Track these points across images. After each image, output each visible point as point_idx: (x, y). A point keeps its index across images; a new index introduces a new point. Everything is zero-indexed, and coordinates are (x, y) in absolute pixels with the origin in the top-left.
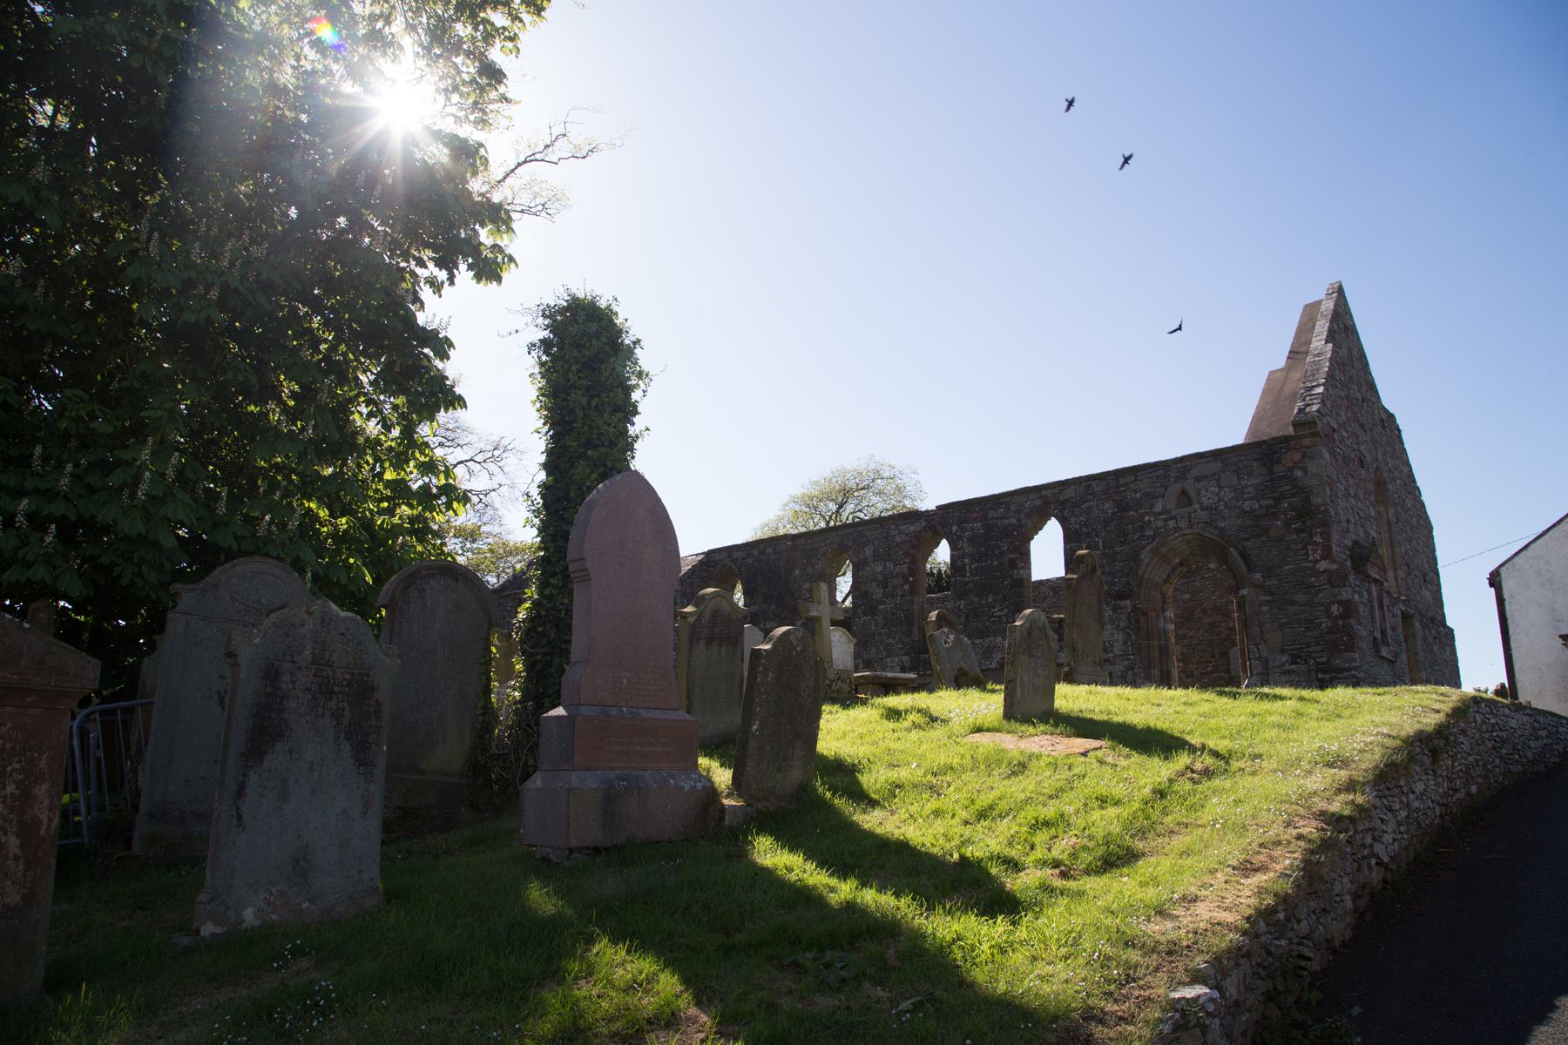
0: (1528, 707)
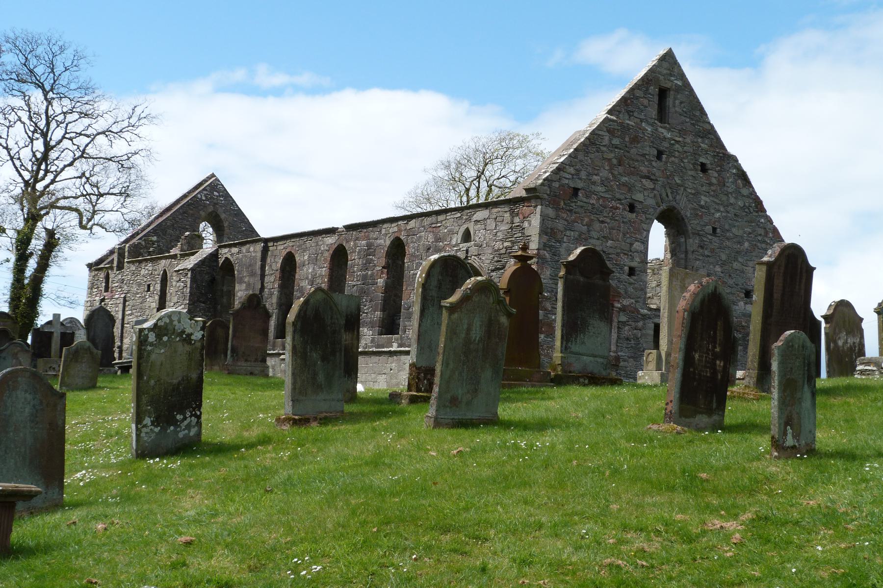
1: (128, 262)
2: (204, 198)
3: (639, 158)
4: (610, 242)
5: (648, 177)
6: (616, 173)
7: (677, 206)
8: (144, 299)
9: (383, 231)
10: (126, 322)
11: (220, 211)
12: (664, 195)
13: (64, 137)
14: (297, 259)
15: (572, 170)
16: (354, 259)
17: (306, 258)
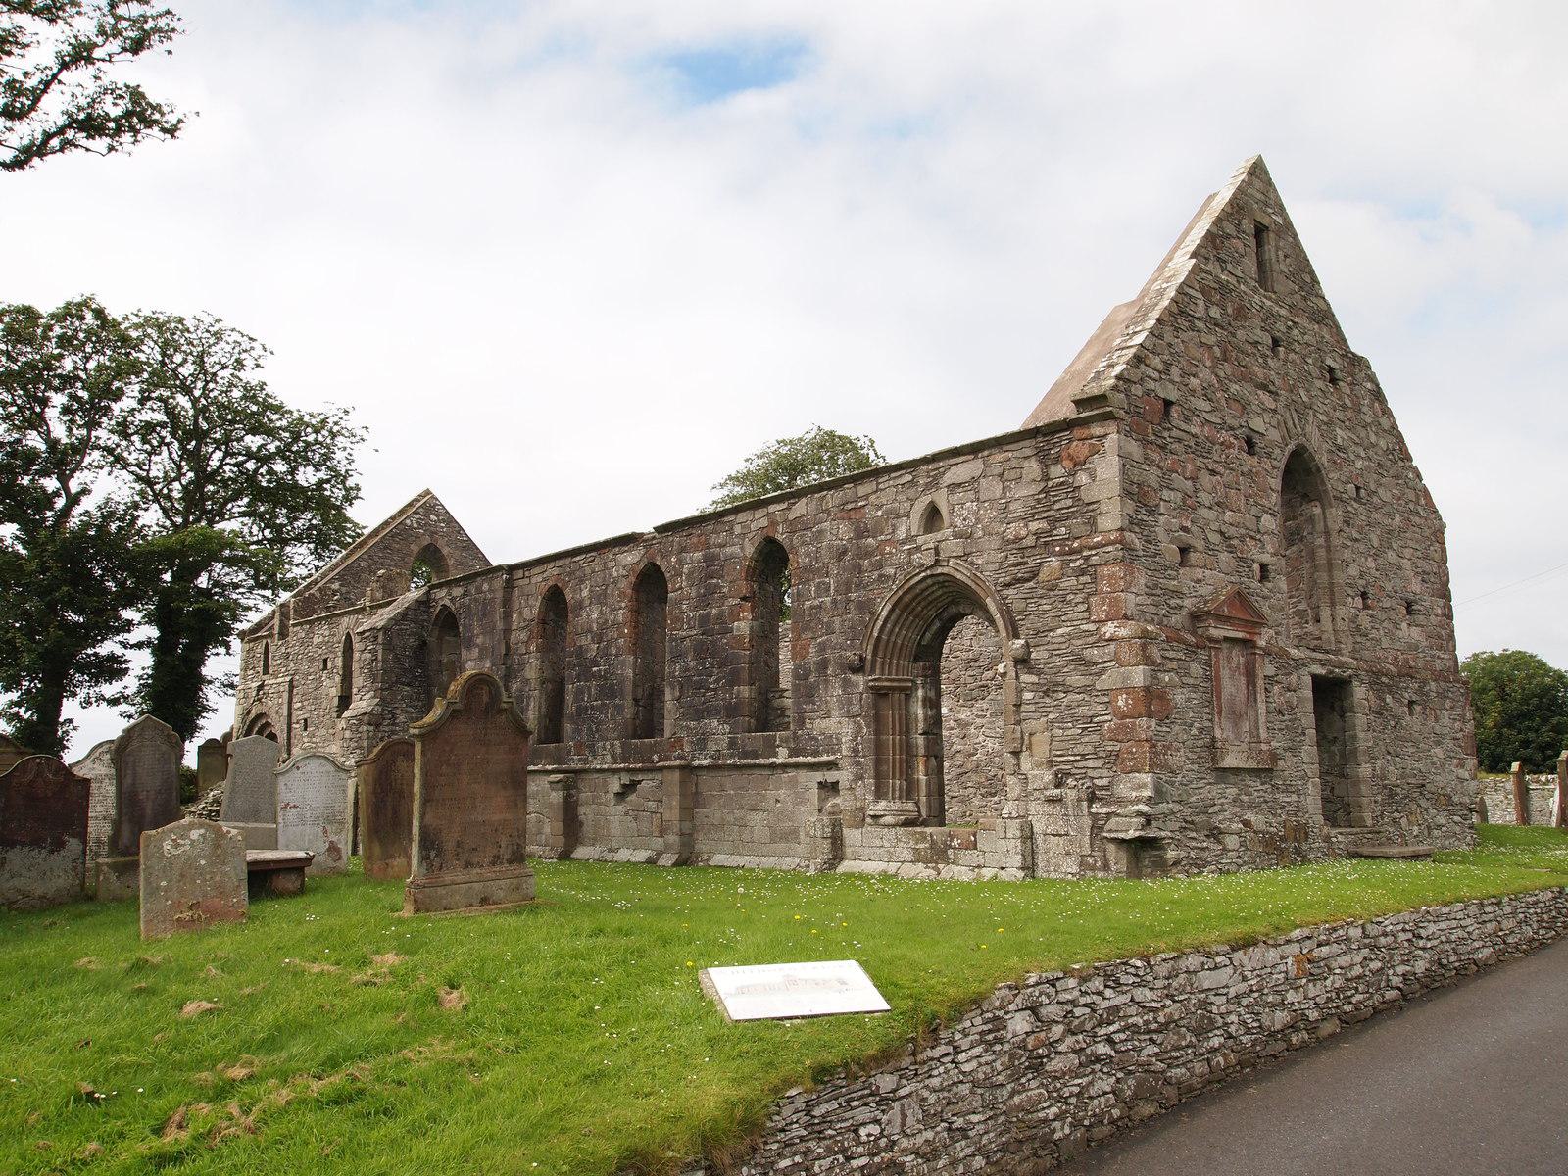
0: (500, 568)
1: (294, 626)
2: (415, 526)
3: (1250, 348)
4: (1228, 513)
5: (1264, 387)
6: (1222, 374)
7: (1307, 444)
9: (738, 530)
10: (294, 720)
11: (441, 543)
12: (1290, 424)
14: (569, 596)
15: (1156, 361)
16: (682, 590)
17: (585, 593)
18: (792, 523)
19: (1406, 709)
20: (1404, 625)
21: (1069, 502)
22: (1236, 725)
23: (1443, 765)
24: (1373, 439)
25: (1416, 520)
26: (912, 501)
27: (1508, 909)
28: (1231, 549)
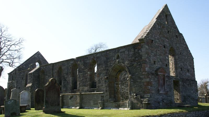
3: (164, 32)
4: (161, 56)
5: (167, 38)
6: (160, 36)
8: (22, 82)
13: (4, 47)
18: (97, 57)
19: (187, 85)
20: (187, 73)
21: (138, 55)
22: (162, 87)
23: (193, 94)
24: (183, 46)
25: (189, 57)
26: (115, 54)
27: (200, 113)
28: (161, 62)
